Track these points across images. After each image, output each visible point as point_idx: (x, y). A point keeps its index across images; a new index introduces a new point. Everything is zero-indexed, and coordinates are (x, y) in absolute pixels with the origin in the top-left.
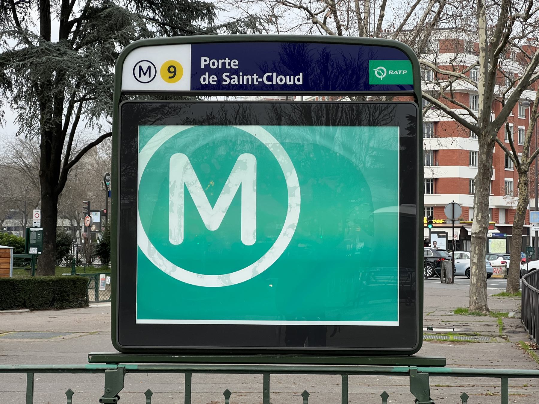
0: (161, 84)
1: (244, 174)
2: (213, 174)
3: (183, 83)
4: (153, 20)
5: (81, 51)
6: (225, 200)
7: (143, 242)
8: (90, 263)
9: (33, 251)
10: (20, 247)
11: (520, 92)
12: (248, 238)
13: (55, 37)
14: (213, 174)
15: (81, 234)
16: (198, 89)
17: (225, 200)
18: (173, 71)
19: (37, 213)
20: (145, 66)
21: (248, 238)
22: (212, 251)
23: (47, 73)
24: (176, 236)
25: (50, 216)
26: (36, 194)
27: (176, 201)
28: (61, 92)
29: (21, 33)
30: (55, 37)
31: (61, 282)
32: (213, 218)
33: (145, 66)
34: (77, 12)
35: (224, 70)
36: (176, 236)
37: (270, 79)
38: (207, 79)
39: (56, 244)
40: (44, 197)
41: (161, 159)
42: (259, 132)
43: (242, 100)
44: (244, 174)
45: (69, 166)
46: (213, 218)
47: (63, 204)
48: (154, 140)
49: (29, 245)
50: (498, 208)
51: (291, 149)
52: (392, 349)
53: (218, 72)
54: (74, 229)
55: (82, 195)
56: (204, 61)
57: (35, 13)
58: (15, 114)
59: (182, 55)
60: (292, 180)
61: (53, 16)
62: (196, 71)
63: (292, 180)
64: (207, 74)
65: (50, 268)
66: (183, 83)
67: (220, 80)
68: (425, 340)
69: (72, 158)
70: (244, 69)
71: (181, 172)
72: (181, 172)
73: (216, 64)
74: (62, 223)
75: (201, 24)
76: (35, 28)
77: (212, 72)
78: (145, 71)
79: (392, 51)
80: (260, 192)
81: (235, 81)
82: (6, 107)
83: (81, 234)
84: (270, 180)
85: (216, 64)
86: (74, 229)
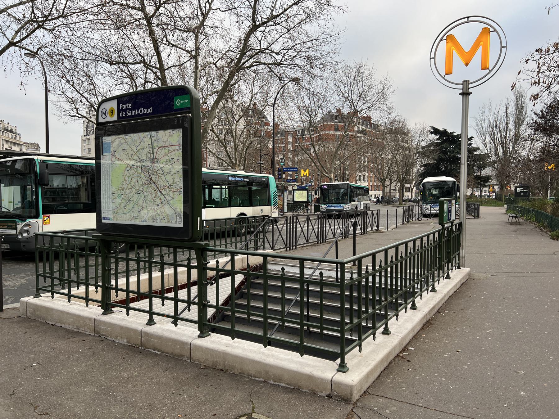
0: (109, 119)
3: (115, 118)
35: (127, 109)
37: (141, 111)
38: (122, 114)
56: (121, 106)
62: (119, 111)
66: (115, 118)
70: (134, 108)
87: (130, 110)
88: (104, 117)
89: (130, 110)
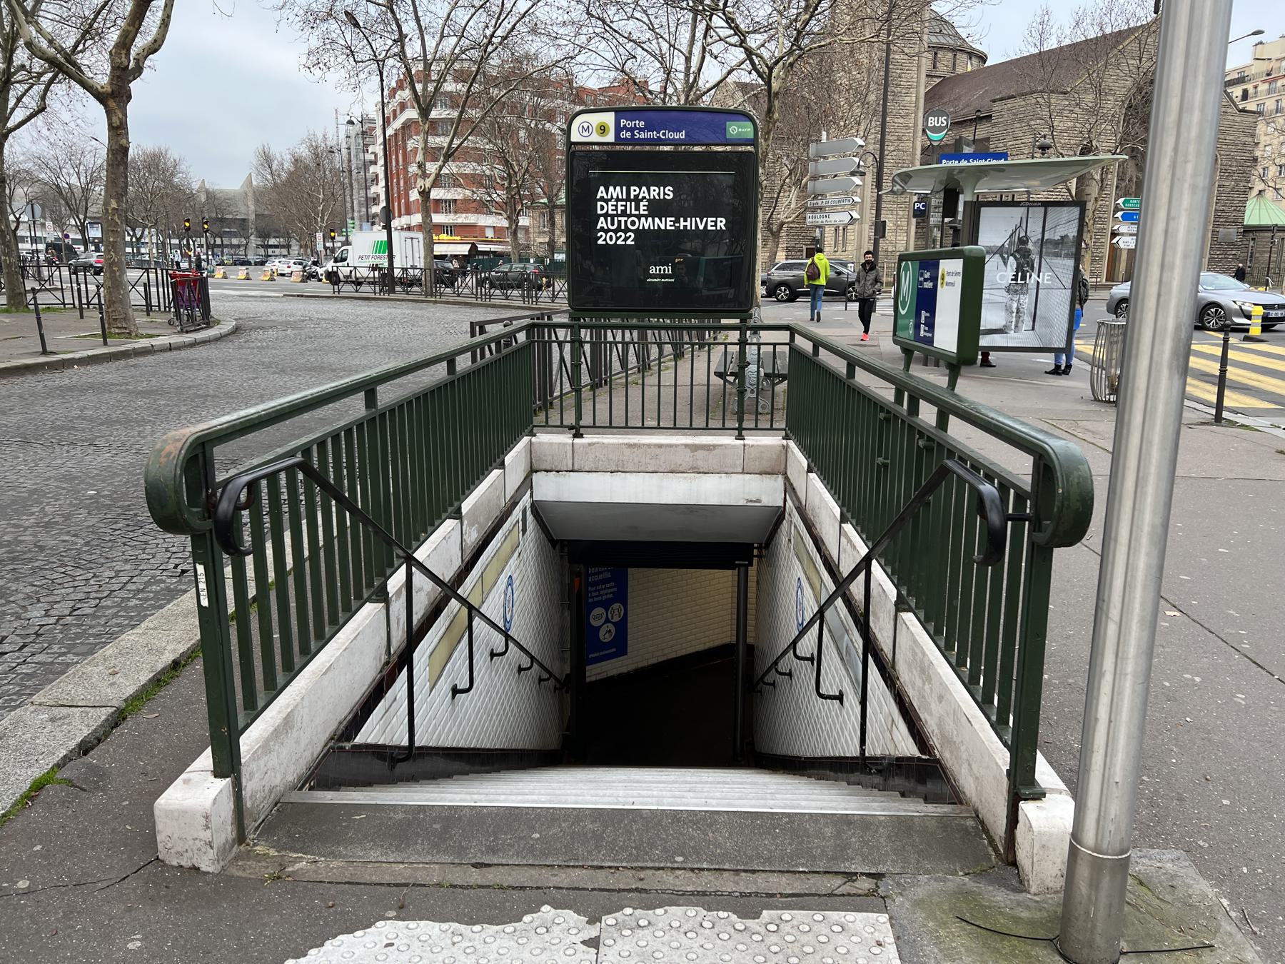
0: (595, 138)
3: (610, 138)
11: (405, 148)
16: (619, 140)
18: (603, 129)
20: (586, 125)
33: (586, 125)
35: (635, 128)
38: (625, 135)
43: (460, 221)
53: (632, 130)
59: (609, 119)
62: (618, 129)
64: (602, 188)
66: (610, 138)
67: (633, 135)
68: (957, 274)
70: (649, 128)
73: (630, 124)
77: (628, 130)
78: (783, 367)
81: (642, 136)
85: (630, 124)
87: (641, 130)
88: (586, 134)
89: (641, 130)
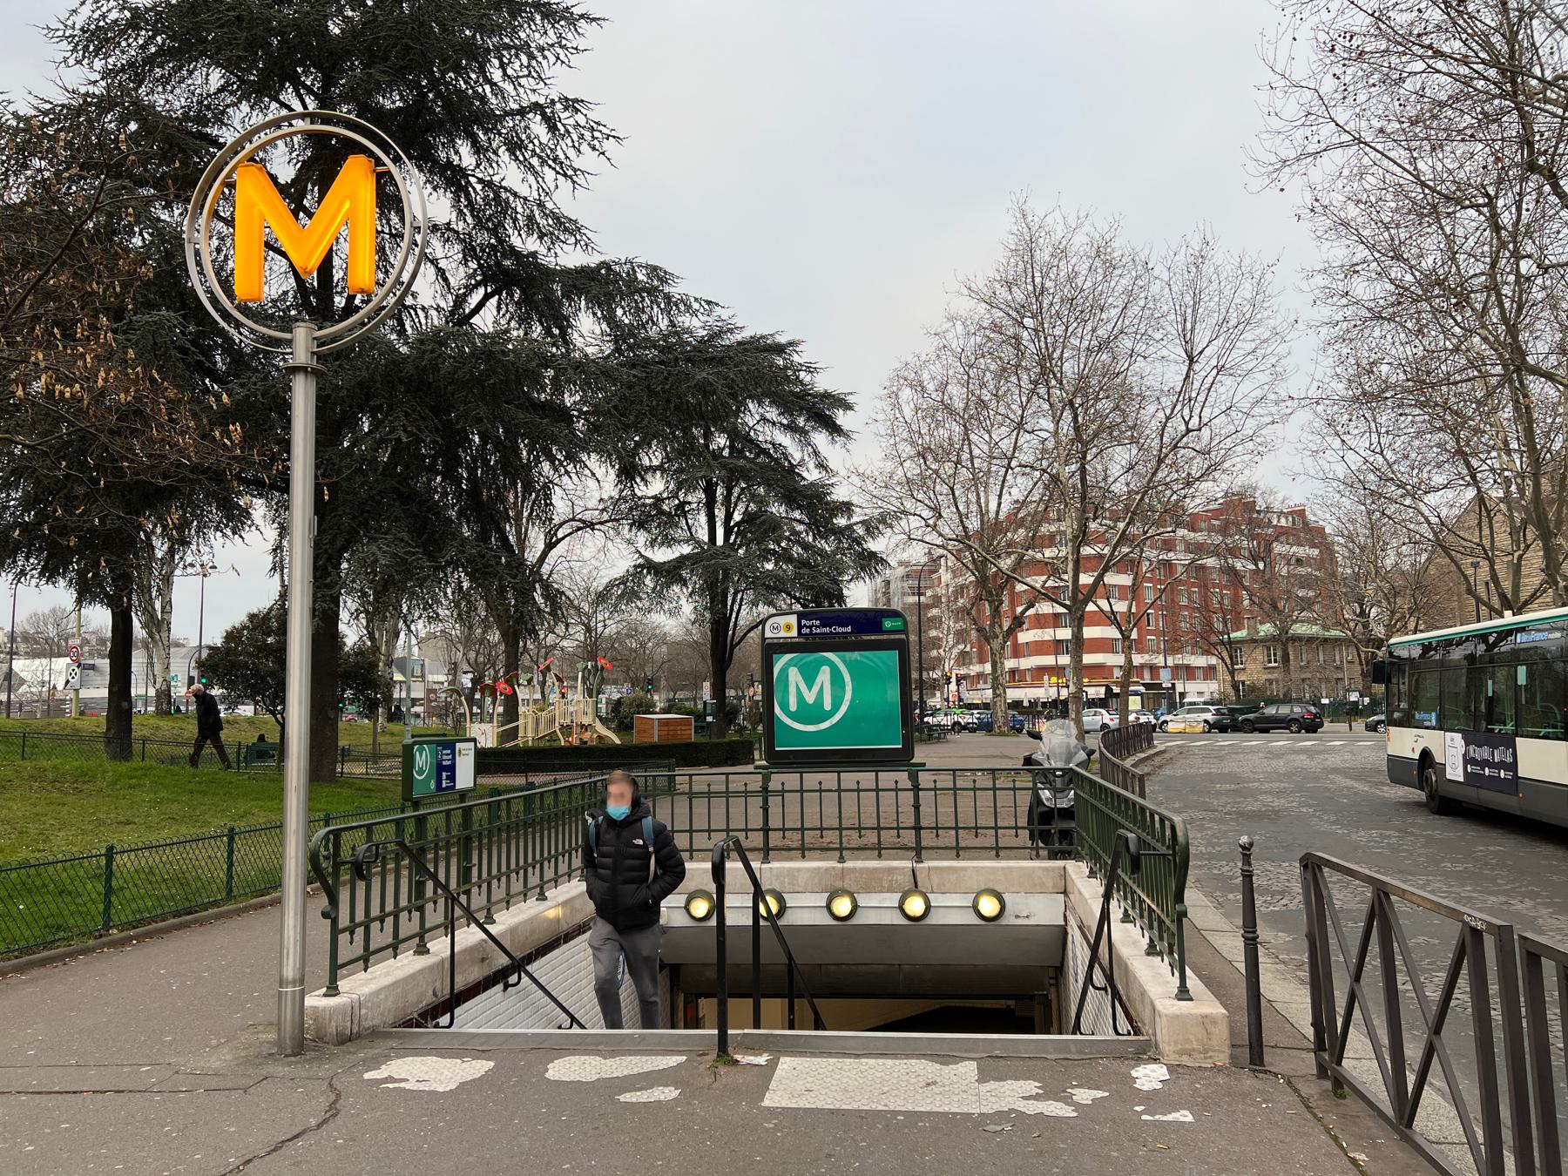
0: (783, 634)
1: (824, 676)
2: (810, 680)
3: (794, 633)
4: (800, 522)
5: (741, 551)
6: (816, 688)
7: (777, 710)
8: (754, 729)
9: (709, 719)
10: (700, 717)
12: (828, 707)
13: (720, 541)
14: (810, 680)
15: (746, 703)
17: (816, 688)
18: (789, 627)
19: (707, 685)
21: (828, 707)
22: (811, 713)
23: (716, 572)
24: (793, 707)
25: (719, 690)
26: (706, 667)
27: (792, 690)
28: (727, 588)
29: (692, 538)
30: (720, 541)
31: (732, 743)
32: (810, 698)
34: (737, 517)
36: (793, 707)
38: (805, 631)
39: (726, 712)
40: (715, 673)
41: (784, 670)
42: (830, 655)
44: (824, 676)
45: (733, 647)
46: (810, 698)
47: (730, 675)
48: (781, 661)
49: (706, 715)
50: (1142, 666)
51: (847, 664)
52: (899, 759)
54: (740, 698)
55: (745, 667)
57: (703, 518)
58: (691, 607)
60: (847, 678)
61: (718, 524)
62: (800, 627)
63: (847, 678)
65: (722, 733)
69: (737, 640)
71: (794, 674)
72: (794, 674)
73: (809, 623)
74: (731, 693)
75: (841, 521)
76: (703, 534)
78: (776, 628)
79: (895, 614)
80: (832, 685)
82: (683, 601)
83: (746, 703)
84: (836, 678)
85: (809, 623)
86: (740, 698)
